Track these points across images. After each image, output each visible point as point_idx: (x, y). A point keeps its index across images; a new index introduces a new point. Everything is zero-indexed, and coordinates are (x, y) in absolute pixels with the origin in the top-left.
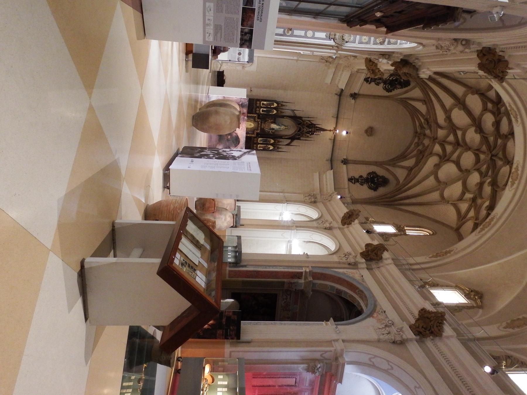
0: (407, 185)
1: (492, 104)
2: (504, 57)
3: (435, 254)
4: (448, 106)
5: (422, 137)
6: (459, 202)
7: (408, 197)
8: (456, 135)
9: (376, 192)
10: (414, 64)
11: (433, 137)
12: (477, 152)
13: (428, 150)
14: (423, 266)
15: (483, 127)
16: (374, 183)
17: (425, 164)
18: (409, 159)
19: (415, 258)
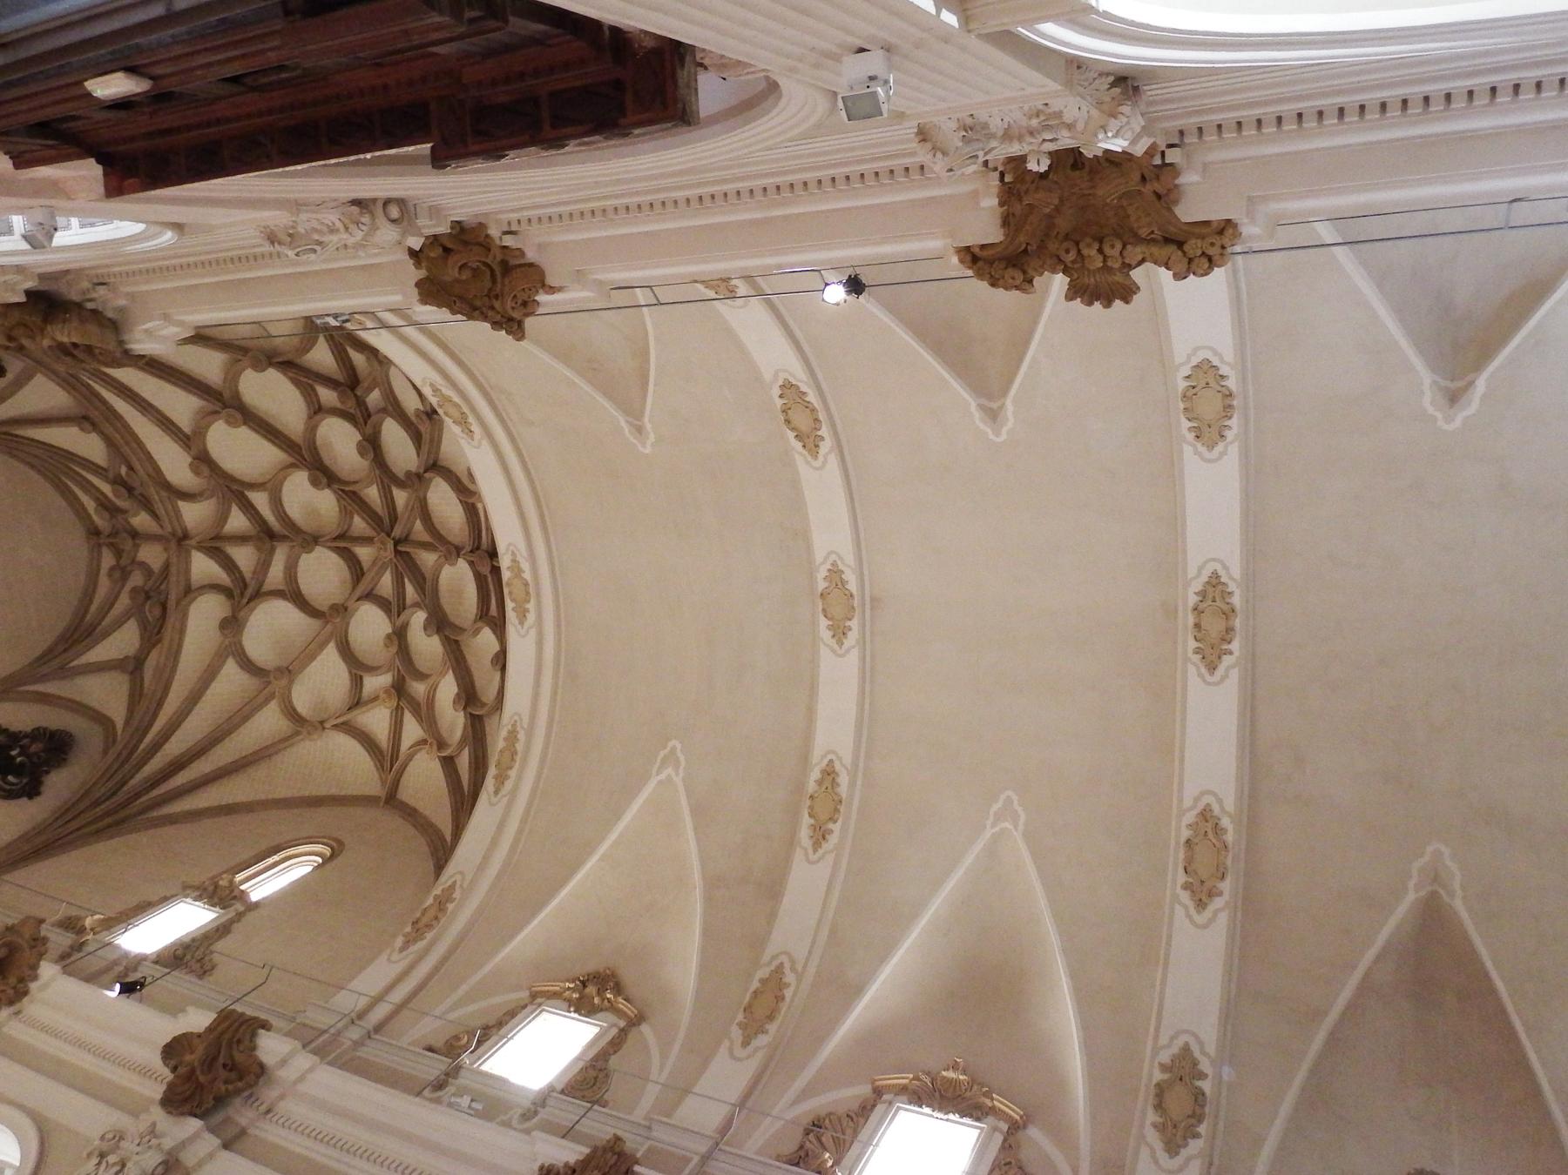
0: (150, 725)
1: (334, 389)
2: (521, 252)
3: (408, 929)
4: (184, 420)
5: (128, 545)
6: (355, 712)
7: (178, 765)
8: (249, 508)
9: (38, 799)
10: (90, 306)
11: (174, 534)
12: (342, 544)
13: (173, 579)
14: (397, 996)
15: (327, 462)
16: (18, 771)
17: (182, 631)
18: (106, 634)
19: (356, 984)
